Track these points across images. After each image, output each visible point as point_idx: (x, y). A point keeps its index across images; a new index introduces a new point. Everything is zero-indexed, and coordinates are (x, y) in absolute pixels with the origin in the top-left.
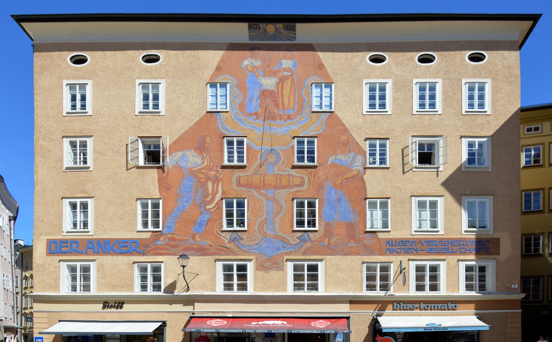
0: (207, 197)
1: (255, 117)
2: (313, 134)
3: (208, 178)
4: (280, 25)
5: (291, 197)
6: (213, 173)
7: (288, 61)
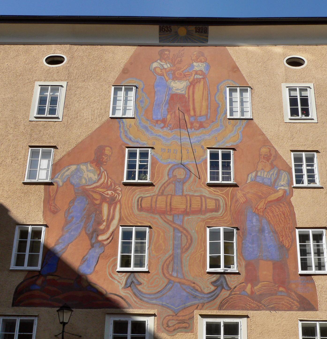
0: (100, 224)
1: (162, 125)
2: (228, 145)
3: (104, 199)
4: (192, 28)
6: (110, 192)
7: (200, 64)
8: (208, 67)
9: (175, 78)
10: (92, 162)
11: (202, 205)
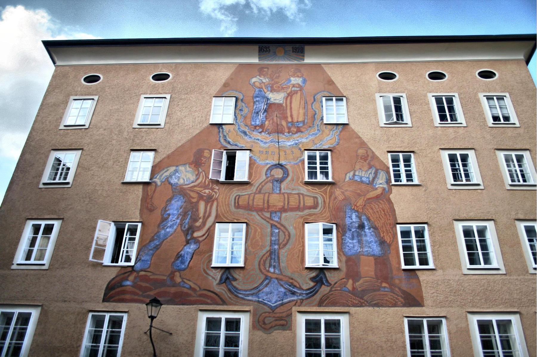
1: (260, 130)
3: (201, 197)
6: (207, 191)
7: (297, 79)
8: (304, 81)
10: (190, 164)
11: (300, 202)
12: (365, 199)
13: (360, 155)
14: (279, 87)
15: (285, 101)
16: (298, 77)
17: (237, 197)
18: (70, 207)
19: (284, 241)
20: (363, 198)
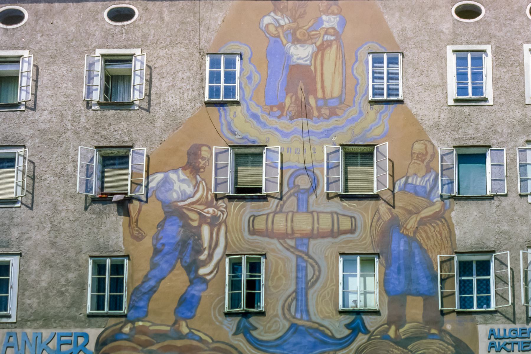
5: (337, 250)
6: (211, 210)
7: (332, 17)
8: (343, 23)
9: (296, 41)
10: (184, 169)
12: (418, 219)
13: (417, 152)
14: (304, 35)
15: (313, 62)
16: (333, 13)
17: (252, 218)
18: (26, 236)
19: (313, 278)
20: (414, 216)
